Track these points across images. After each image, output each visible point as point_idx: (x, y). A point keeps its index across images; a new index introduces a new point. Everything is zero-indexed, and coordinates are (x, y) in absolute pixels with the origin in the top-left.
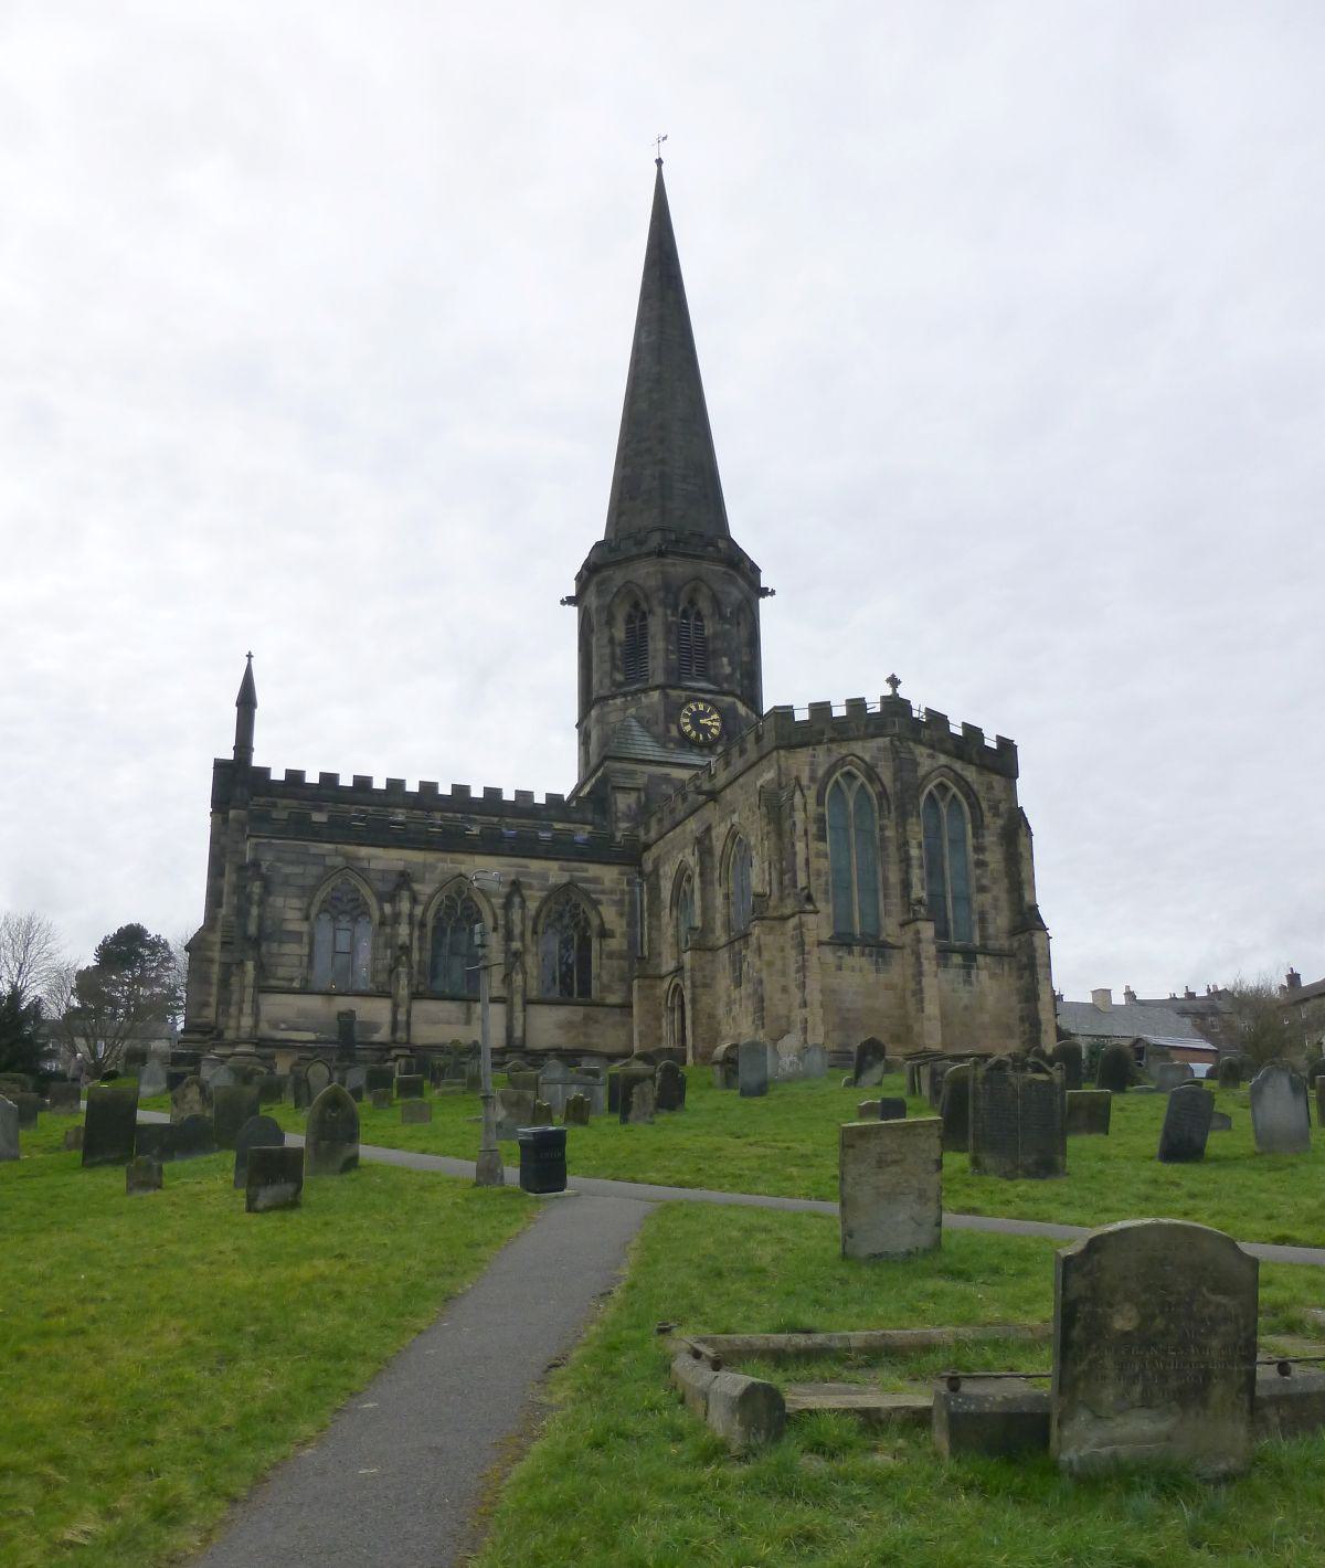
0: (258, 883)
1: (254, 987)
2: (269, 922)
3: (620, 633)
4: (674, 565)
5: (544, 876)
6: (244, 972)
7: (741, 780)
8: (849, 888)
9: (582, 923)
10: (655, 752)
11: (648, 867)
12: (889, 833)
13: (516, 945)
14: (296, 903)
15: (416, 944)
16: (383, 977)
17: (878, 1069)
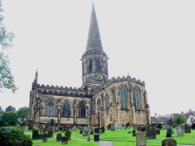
3: (88, 65)
5: (79, 100)
8: (123, 102)
11: (93, 98)
13: (75, 110)
14: (44, 103)
15: (61, 109)
16: (56, 114)
17: (129, 126)
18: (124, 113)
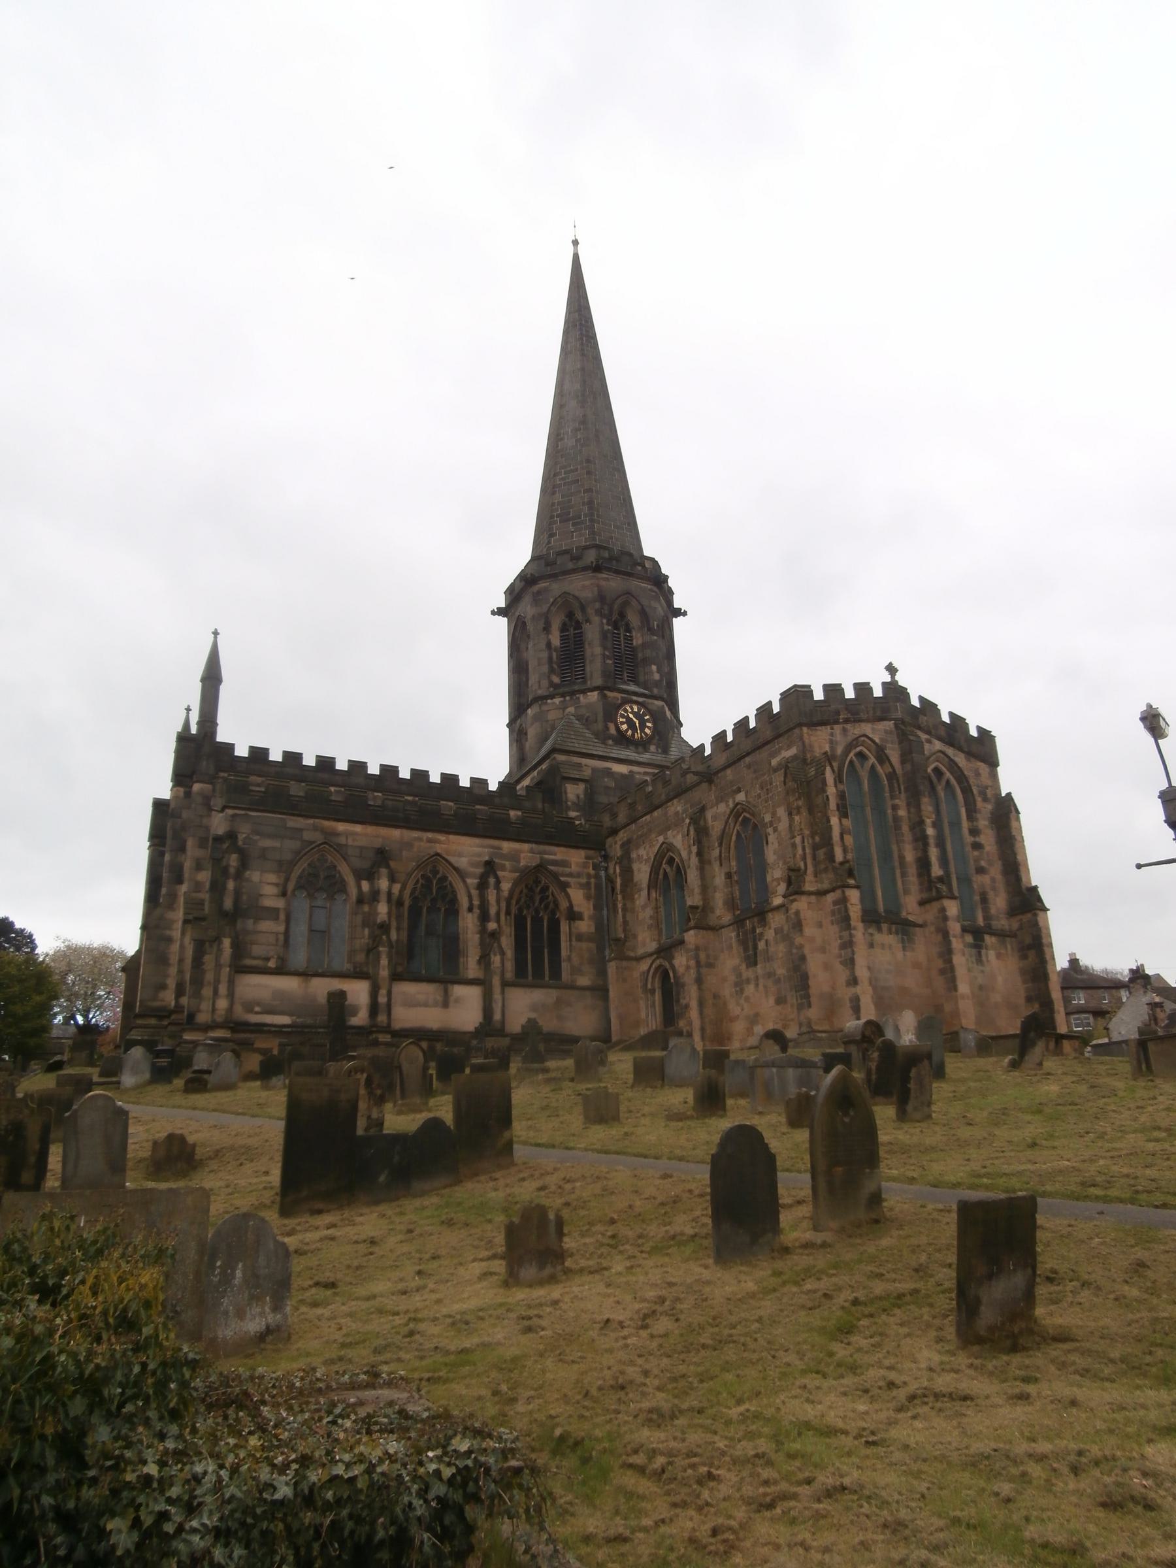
0: (234, 856)
1: (230, 966)
2: (245, 897)
3: (556, 641)
4: (607, 579)
6: (220, 950)
7: (747, 759)
9: (552, 905)
11: (616, 850)
12: (902, 813)
13: (492, 926)
14: (272, 878)
15: (394, 924)
16: (360, 957)
18: (883, 946)
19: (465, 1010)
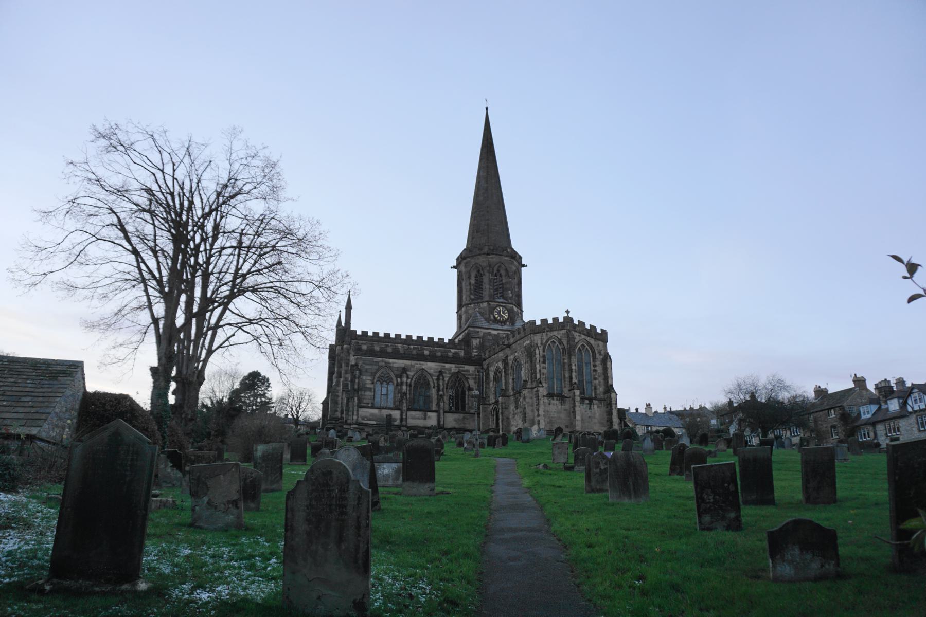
3: (473, 281)
10: (486, 325)
11: (485, 367)
13: (441, 393)
14: (369, 378)
16: (397, 403)
19: (432, 420)
